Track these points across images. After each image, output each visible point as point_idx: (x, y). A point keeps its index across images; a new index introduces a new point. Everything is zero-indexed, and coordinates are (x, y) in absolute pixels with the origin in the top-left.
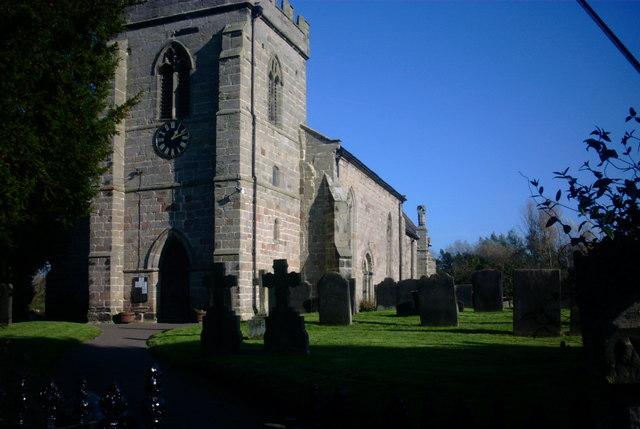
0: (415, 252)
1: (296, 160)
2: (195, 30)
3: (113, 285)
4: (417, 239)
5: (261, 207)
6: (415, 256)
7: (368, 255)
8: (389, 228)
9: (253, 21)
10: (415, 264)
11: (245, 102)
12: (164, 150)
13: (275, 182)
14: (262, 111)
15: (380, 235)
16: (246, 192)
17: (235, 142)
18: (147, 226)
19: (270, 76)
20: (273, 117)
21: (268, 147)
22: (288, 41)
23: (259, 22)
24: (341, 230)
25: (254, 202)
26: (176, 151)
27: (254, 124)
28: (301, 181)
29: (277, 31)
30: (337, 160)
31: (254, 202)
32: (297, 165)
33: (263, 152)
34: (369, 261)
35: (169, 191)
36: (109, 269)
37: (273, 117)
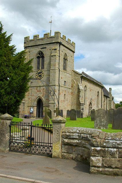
0: (108, 101)
1: (71, 79)
2: (46, 48)
3: (25, 109)
4: (109, 97)
5: (61, 92)
6: (108, 102)
7: (90, 103)
8: (98, 95)
9: (59, 46)
10: (9, 176)
11: (57, 66)
12: (39, 71)
13: (65, 85)
14: (61, 68)
15: (95, 97)
16: (57, 88)
17: (54, 76)
18: (33, 95)
19: (64, 59)
20: (65, 69)
21: (63, 76)
22: (69, 49)
23: (61, 46)
24: (81, 97)
25: (59, 90)
26: (41, 77)
27: (59, 71)
28: (72, 85)
29: (66, 47)
30: (81, 79)
31: (59, 90)
32: (71, 80)
33: (62, 78)
34: (91, 104)
35: (35, 107)
36: (24, 105)
37: (65, 69)
